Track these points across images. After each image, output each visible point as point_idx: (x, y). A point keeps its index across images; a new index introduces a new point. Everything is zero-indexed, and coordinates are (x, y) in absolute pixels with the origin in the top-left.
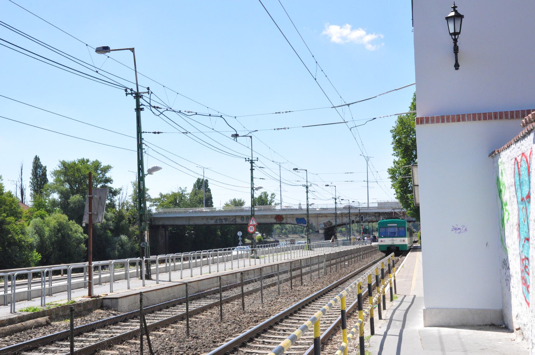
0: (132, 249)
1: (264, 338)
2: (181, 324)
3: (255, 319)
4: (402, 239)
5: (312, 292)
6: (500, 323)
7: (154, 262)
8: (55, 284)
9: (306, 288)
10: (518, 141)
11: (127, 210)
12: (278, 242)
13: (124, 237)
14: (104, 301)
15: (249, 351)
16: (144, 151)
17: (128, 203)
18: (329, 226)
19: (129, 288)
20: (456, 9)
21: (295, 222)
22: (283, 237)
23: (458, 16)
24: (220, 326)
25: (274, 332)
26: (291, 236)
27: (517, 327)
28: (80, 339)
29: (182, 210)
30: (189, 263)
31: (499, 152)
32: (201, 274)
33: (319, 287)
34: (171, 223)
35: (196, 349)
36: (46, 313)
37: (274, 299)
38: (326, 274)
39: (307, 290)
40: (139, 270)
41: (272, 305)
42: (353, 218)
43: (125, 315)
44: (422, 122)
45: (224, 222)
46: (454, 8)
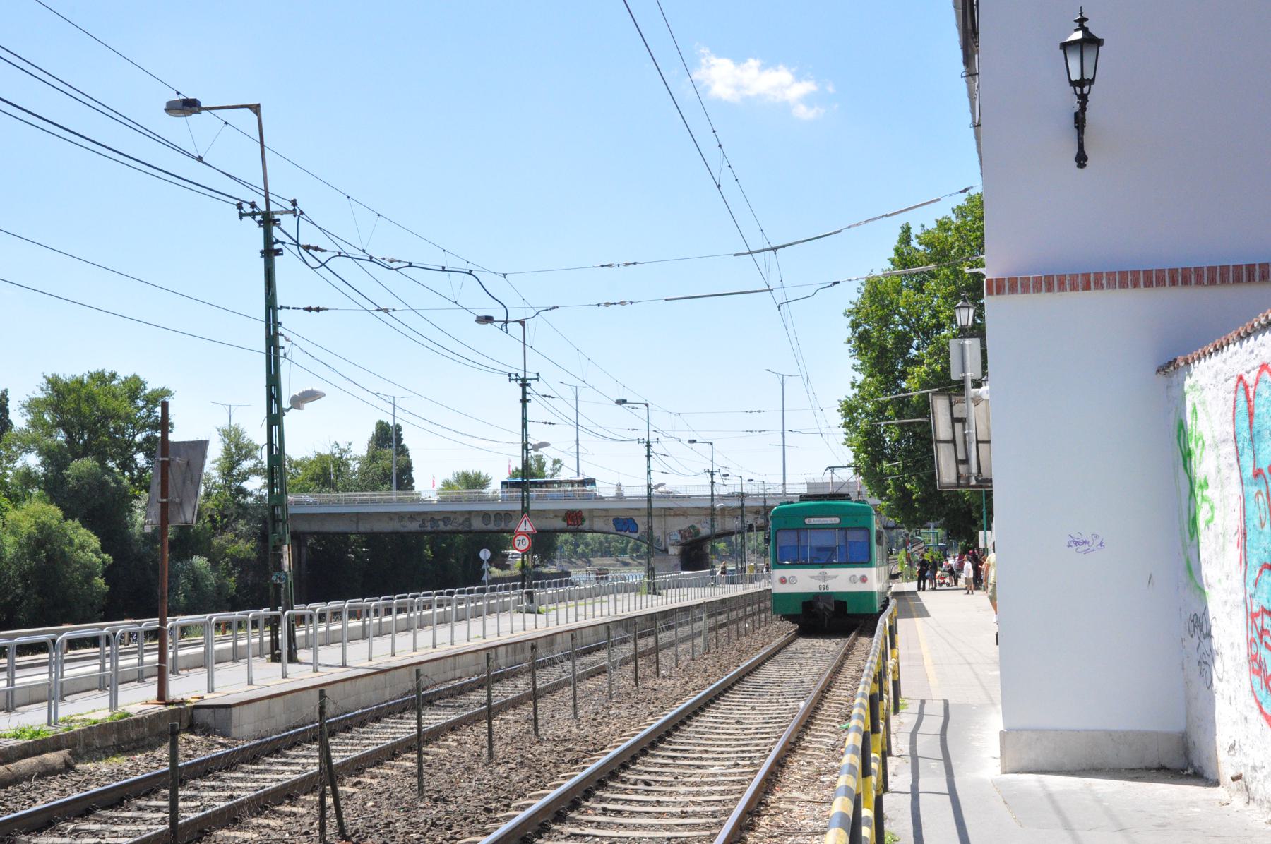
0: (220, 588)
1: (603, 800)
2: (393, 767)
3: (569, 756)
4: (859, 572)
5: (686, 693)
6: (1181, 760)
7: (301, 619)
8: (71, 671)
9: (669, 683)
10: (1248, 335)
11: (208, 495)
12: (568, 574)
13: (200, 562)
14: (196, 712)
15: (577, 831)
16: (281, 352)
17: (209, 480)
18: (694, 537)
19: (250, 683)
20: (1086, 24)
21: (613, 529)
22: (580, 562)
23: (1091, 42)
24: (491, 772)
25: (623, 786)
26: (598, 562)
27: (1234, 774)
28: (153, 803)
29: (342, 496)
30: (364, 625)
31: (1187, 363)
32: (415, 650)
33: (700, 681)
34: (316, 527)
35: (449, 828)
36: (64, 742)
37: (600, 708)
38: (707, 650)
39: (676, 688)
40: (267, 639)
41: (600, 724)
42: (750, 519)
43: (250, 747)
44: (1000, 291)
45: (442, 527)
46: (1082, 21)
